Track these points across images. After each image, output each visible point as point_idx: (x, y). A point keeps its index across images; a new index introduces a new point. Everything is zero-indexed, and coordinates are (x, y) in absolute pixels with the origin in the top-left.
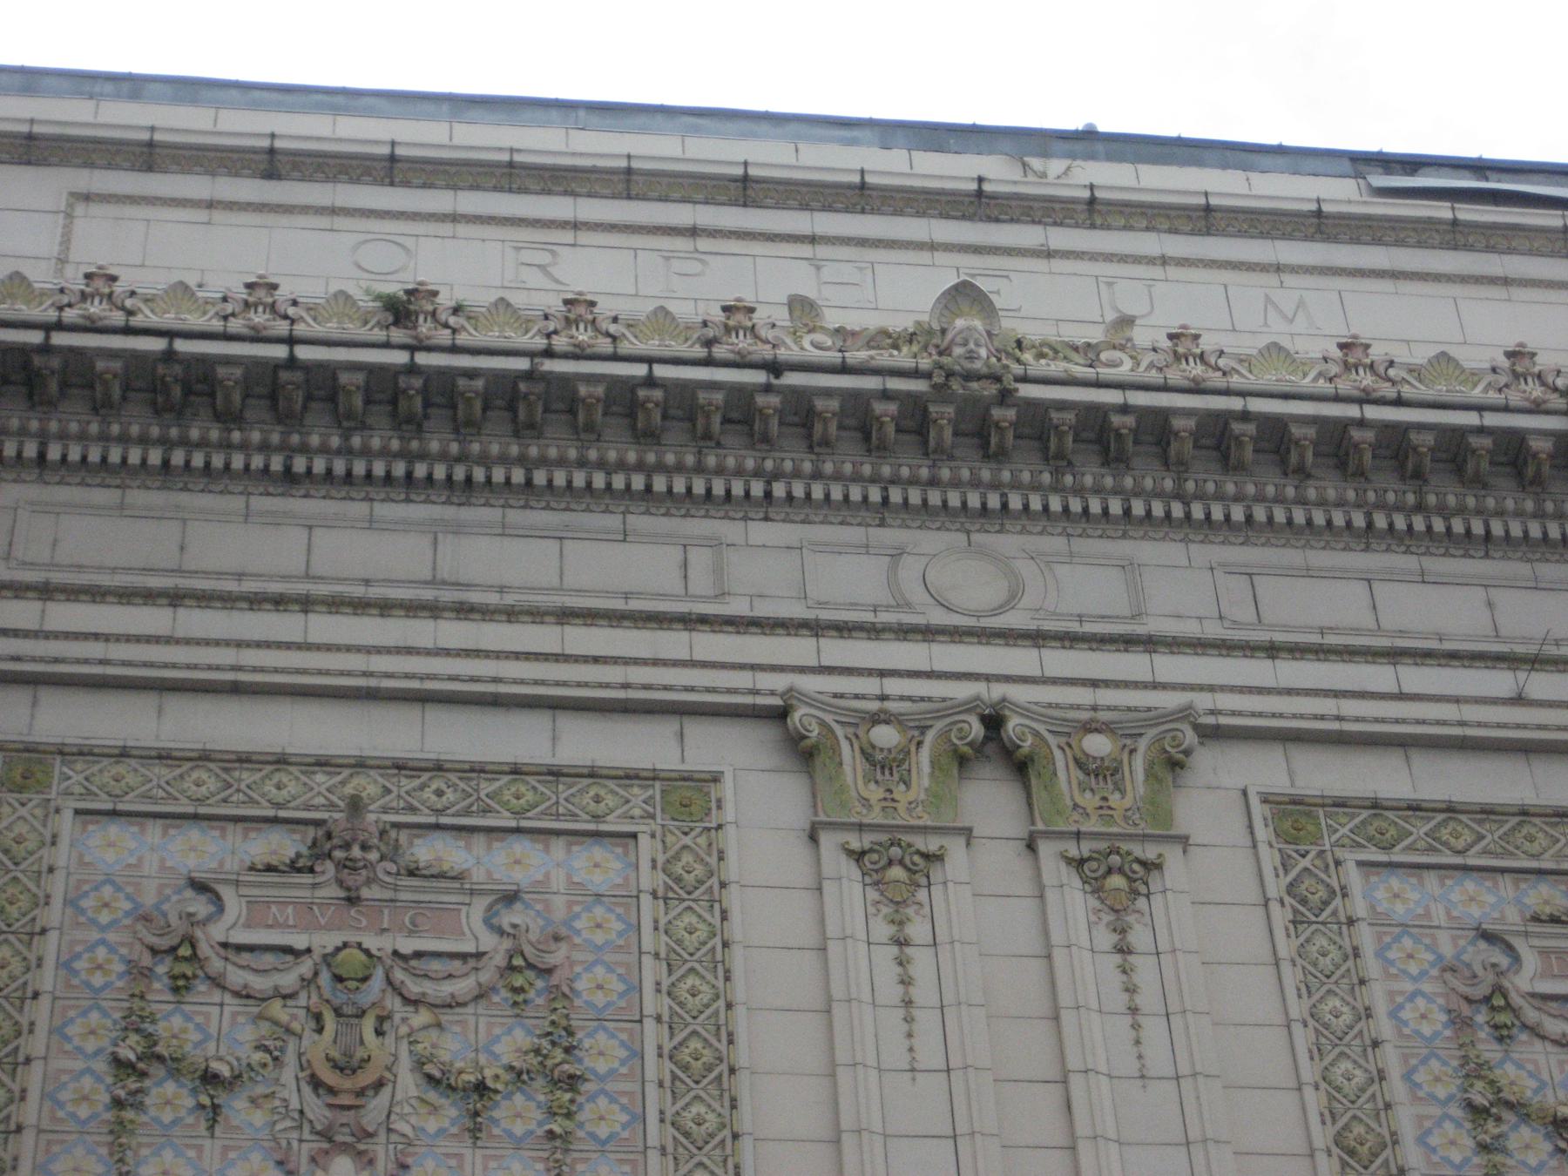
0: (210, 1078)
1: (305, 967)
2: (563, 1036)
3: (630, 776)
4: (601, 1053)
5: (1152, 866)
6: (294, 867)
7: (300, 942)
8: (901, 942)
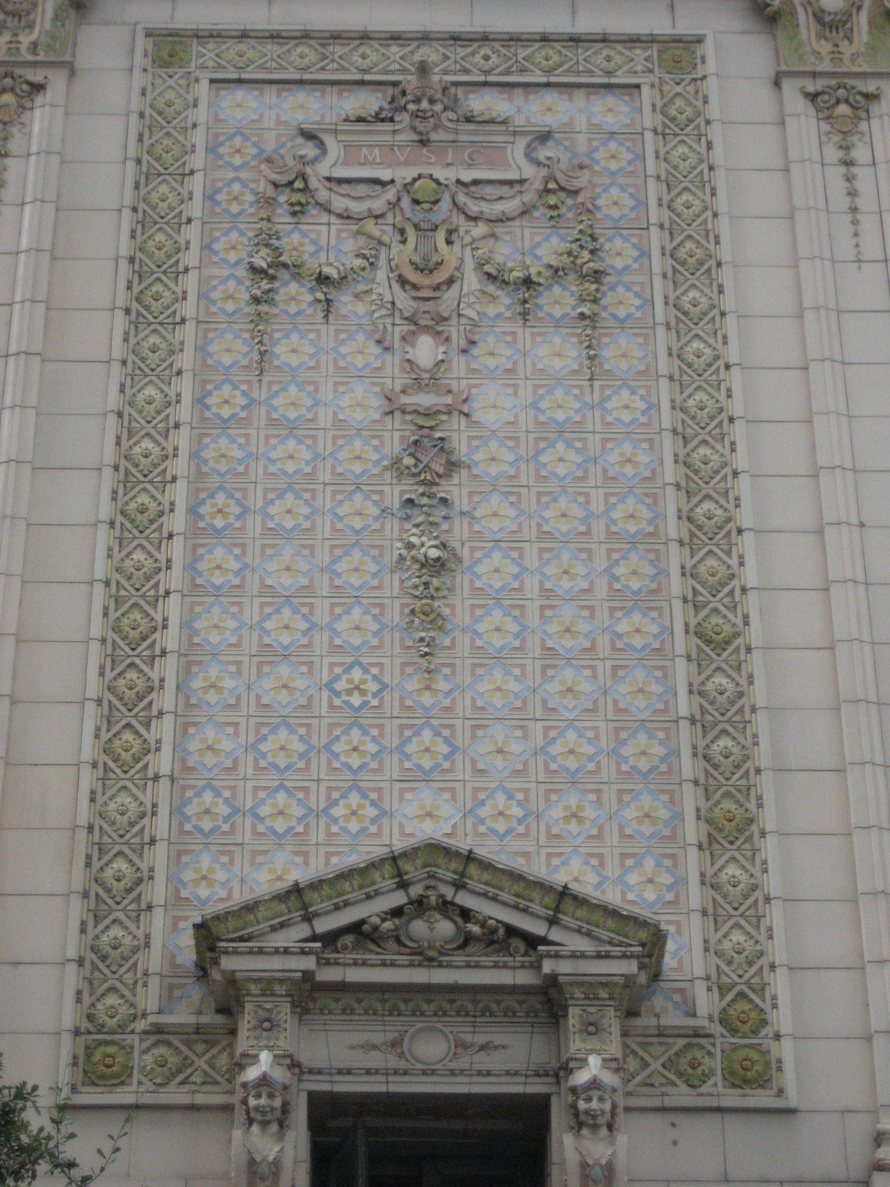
0: (323, 280)
1: (391, 194)
2: (589, 241)
3: (634, 41)
4: (618, 253)
5: (38, 88)
6: (379, 118)
7: (385, 174)
8: (848, 163)
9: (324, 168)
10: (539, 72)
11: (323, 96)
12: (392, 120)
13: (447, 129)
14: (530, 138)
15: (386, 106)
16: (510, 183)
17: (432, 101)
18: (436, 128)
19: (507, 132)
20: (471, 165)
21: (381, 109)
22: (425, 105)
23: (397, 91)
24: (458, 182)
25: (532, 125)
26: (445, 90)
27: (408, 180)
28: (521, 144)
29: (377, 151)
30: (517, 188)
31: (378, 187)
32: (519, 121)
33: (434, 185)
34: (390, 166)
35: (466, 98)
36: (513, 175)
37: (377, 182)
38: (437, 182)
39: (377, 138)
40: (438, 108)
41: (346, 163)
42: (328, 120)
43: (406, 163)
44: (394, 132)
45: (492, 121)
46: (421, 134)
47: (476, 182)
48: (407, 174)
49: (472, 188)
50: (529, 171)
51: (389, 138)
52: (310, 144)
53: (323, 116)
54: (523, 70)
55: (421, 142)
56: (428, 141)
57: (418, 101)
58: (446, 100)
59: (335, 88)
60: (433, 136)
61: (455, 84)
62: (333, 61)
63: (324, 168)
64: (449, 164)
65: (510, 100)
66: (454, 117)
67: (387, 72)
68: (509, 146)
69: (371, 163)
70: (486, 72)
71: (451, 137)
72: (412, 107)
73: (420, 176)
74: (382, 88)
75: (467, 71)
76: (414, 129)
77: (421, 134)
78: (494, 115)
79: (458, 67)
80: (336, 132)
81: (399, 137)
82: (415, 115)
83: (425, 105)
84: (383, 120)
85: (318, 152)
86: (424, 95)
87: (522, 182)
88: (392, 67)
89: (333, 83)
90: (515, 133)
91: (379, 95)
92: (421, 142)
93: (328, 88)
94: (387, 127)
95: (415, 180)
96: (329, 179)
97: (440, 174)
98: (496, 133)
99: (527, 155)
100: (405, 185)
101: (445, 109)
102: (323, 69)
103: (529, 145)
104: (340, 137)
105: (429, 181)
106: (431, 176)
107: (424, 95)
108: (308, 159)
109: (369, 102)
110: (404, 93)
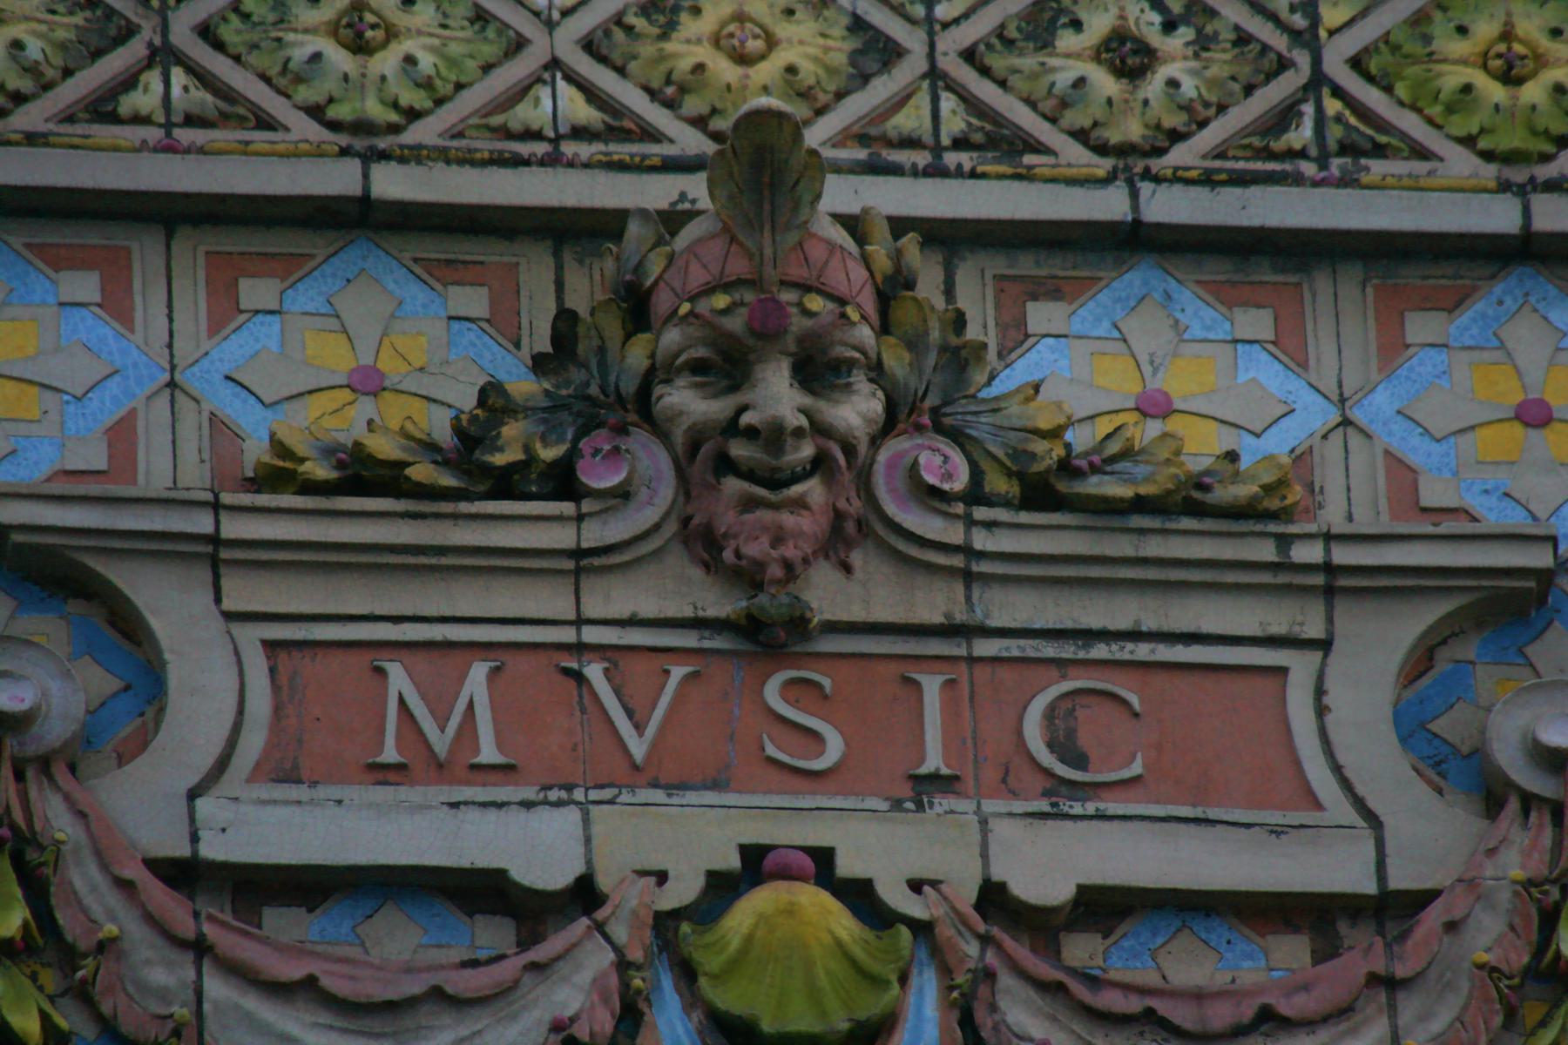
6: (474, 463)
9: (144, 806)
10: (1460, 163)
11: (117, 306)
12: (562, 482)
13: (909, 556)
14: (1428, 614)
15: (523, 385)
16: (1314, 916)
17: (818, 370)
18: (838, 541)
19: (1282, 579)
20: (1064, 794)
21: (494, 402)
22: (777, 394)
23: (586, 289)
24: (994, 898)
25: (1452, 522)
26: (892, 289)
27: (684, 890)
28: (1376, 645)
29: (479, 672)
30: (1363, 951)
31: (493, 934)
32: (1348, 496)
33: (842, 923)
34: (557, 789)
35: (1016, 337)
36: (1342, 869)
37: (481, 892)
38: (859, 896)
39: (467, 598)
40: (857, 410)
41: (285, 769)
42: (154, 472)
43: (666, 776)
44: (582, 563)
45: (1189, 501)
46: (749, 577)
47: (1102, 907)
48: (691, 838)
49: (1081, 949)
50: (1429, 837)
51: (552, 600)
52: (47, 627)
53: (122, 434)
54: (1360, 148)
55: (750, 628)
56: (799, 625)
57: (727, 366)
58: (896, 361)
59: (191, 251)
60: (826, 595)
61: (949, 238)
62: (164, 55)
63: (144, 806)
64: (927, 787)
65: (1290, 348)
66: (945, 466)
67: (509, 146)
68: (1301, 666)
69: (440, 769)
70: (1132, 161)
71: (933, 603)
72: (685, 401)
73: (756, 864)
74: (491, 253)
75: (1004, 146)
76: (704, 544)
77: (749, 577)
78: (1201, 446)
79: (954, 120)
80: (213, 556)
81: (612, 598)
82: (706, 456)
83: (777, 394)
84: (505, 484)
85: (99, 680)
86: (767, 332)
87: (1394, 909)
88: (537, 111)
89: (170, 214)
90: (1333, 584)
91: (473, 301)
92: (750, 628)
93: (145, 251)
94: (540, 527)
95: (722, 889)
96: (183, 874)
97: (878, 848)
98: (1215, 580)
99: (1412, 728)
100: (664, 922)
101: (889, 425)
102: (102, 108)
103: (1421, 661)
104: (242, 593)
105: (814, 900)
106: (823, 858)
107: (767, 332)
108: (54, 731)
109: (410, 353)
110: (635, 306)
